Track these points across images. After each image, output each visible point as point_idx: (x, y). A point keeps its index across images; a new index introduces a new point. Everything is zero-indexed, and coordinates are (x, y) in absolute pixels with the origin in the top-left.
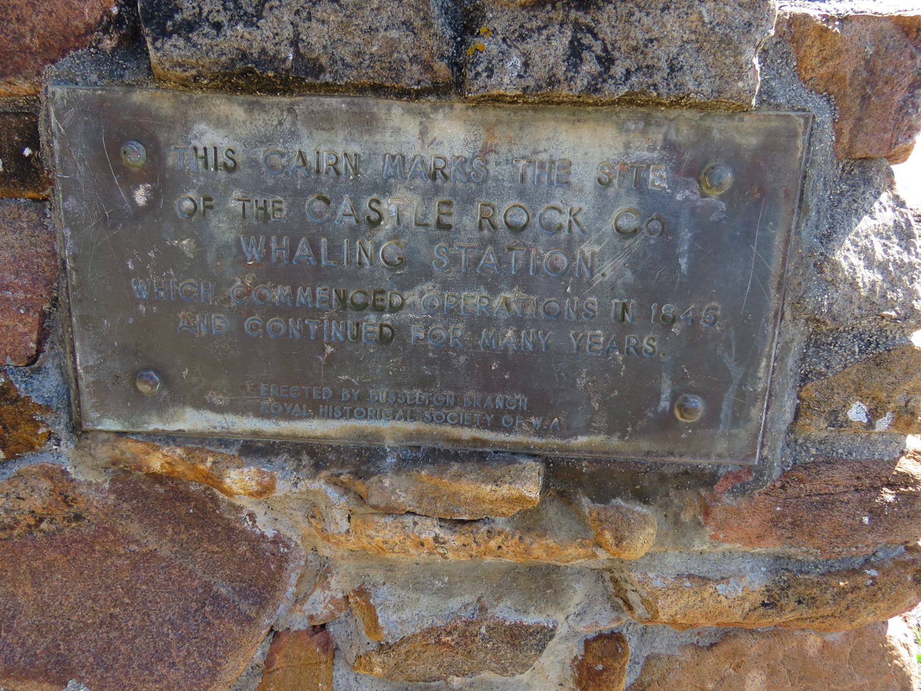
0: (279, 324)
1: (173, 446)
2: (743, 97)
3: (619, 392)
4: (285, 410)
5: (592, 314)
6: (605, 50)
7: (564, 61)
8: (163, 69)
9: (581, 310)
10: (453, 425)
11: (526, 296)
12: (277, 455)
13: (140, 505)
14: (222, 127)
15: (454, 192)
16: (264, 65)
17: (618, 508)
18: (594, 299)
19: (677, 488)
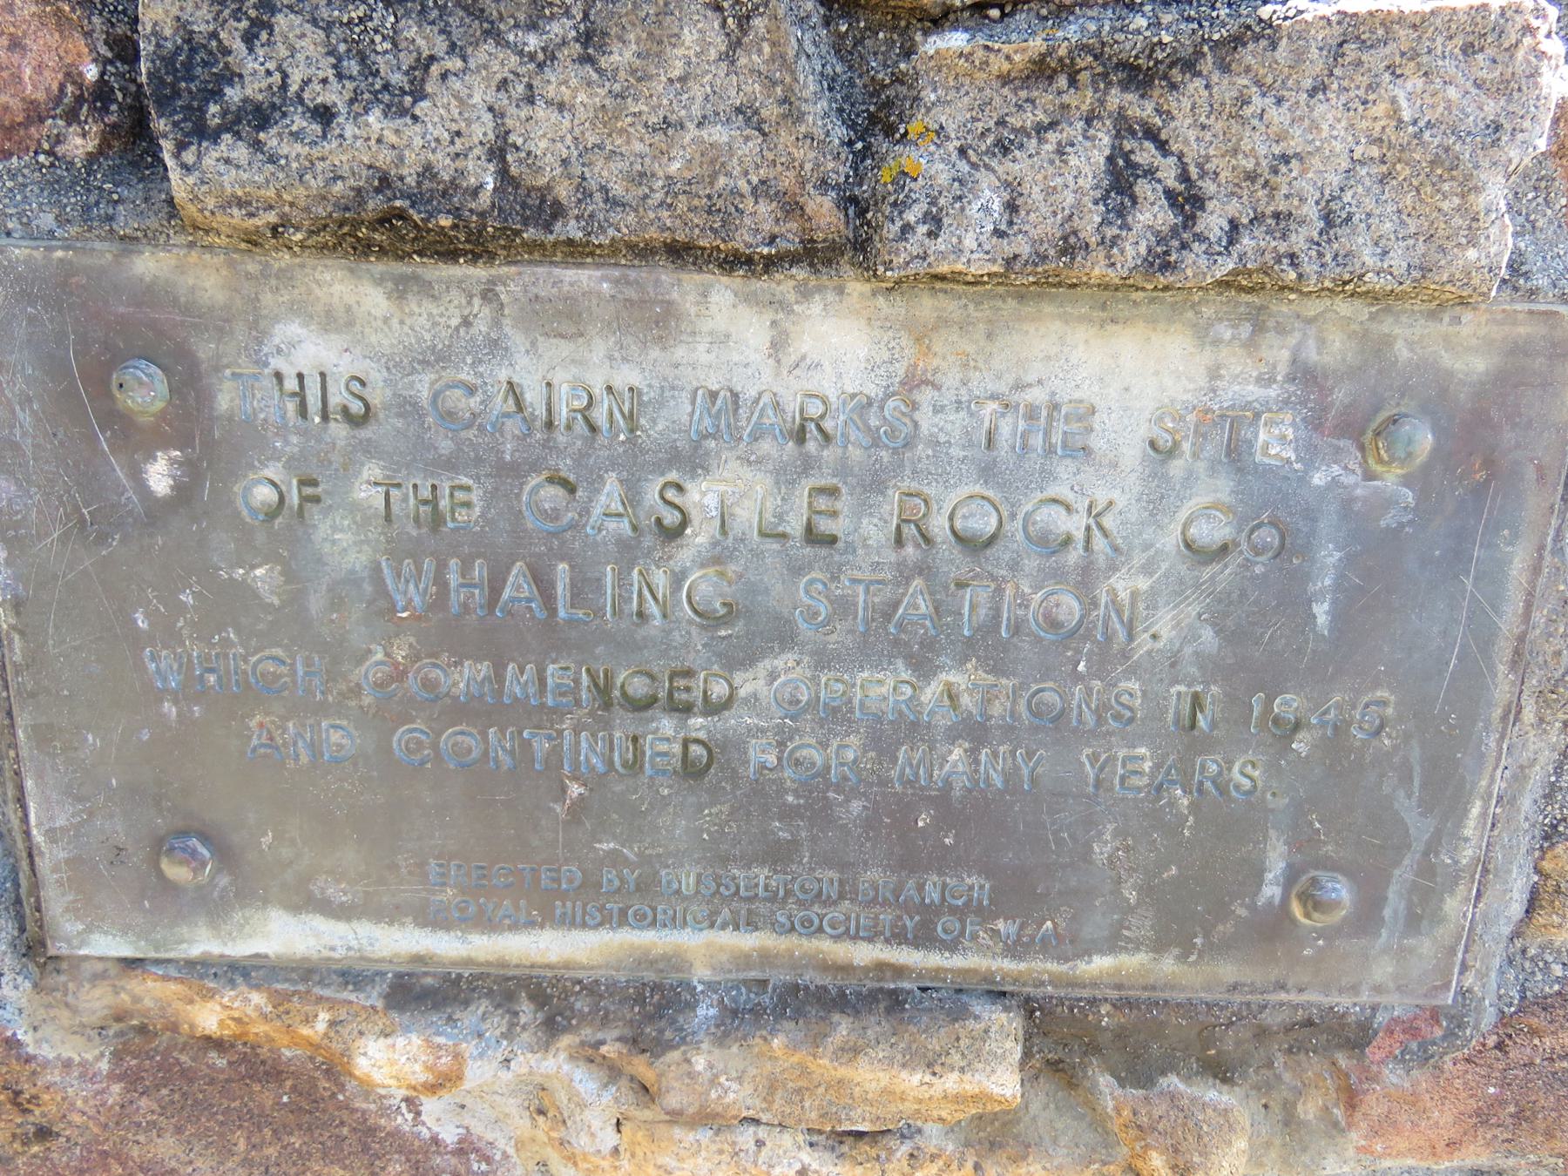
0: (467, 739)
1: (243, 988)
2: (1476, 281)
3: (1179, 868)
4: (481, 911)
5: (1128, 714)
6: (1184, 177)
7: (1096, 203)
8: (201, 211)
9: (1106, 706)
10: (836, 938)
11: (991, 679)
12: (466, 1003)
13: (177, 1097)
14: (338, 331)
15: (843, 469)
16: (429, 201)
17: (1173, 1097)
18: (1134, 685)
19: (1290, 1051)
